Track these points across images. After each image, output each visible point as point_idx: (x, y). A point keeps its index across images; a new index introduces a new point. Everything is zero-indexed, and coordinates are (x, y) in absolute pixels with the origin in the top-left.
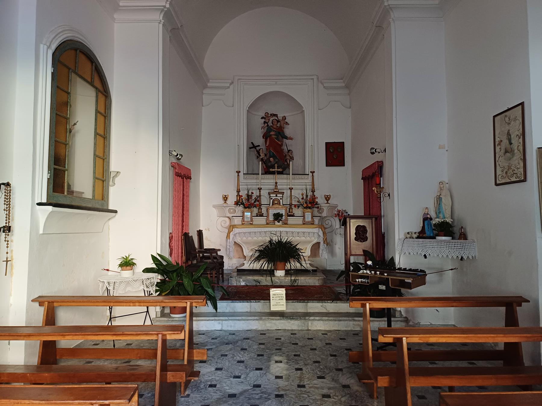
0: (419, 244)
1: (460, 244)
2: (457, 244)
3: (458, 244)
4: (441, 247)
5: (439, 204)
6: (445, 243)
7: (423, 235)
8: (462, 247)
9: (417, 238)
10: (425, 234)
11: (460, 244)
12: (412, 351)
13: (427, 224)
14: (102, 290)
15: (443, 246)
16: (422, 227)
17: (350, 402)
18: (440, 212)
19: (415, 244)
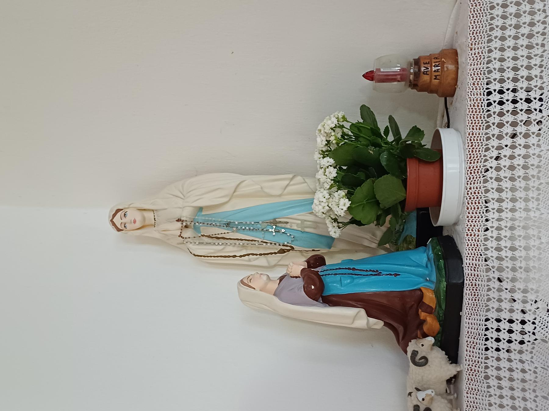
0: (504, 335)
1: (497, 44)
2: (497, 65)
3: (497, 54)
4: (520, 172)
5: (228, 225)
6: (494, 142)
7: (429, 310)
8: (517, 27)
9: (454, 358)
10: (422, 296)
11: (497, 44)
12: (421, 313)
13: (347, 281)
14: (426, 288)
15: (518, 161)
16: (369, 315)
17: (291, 264)
18: (275, 222)
19: (504, 364)
